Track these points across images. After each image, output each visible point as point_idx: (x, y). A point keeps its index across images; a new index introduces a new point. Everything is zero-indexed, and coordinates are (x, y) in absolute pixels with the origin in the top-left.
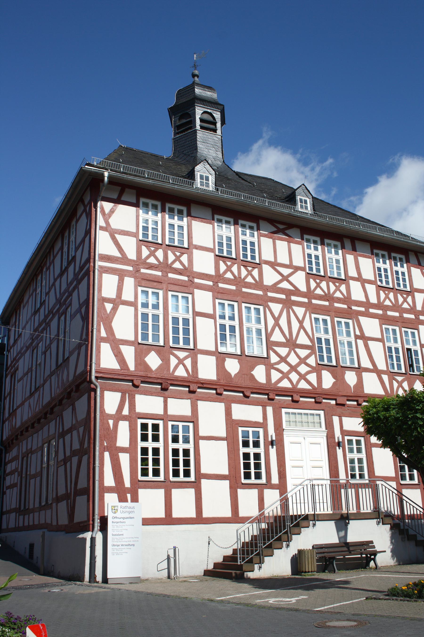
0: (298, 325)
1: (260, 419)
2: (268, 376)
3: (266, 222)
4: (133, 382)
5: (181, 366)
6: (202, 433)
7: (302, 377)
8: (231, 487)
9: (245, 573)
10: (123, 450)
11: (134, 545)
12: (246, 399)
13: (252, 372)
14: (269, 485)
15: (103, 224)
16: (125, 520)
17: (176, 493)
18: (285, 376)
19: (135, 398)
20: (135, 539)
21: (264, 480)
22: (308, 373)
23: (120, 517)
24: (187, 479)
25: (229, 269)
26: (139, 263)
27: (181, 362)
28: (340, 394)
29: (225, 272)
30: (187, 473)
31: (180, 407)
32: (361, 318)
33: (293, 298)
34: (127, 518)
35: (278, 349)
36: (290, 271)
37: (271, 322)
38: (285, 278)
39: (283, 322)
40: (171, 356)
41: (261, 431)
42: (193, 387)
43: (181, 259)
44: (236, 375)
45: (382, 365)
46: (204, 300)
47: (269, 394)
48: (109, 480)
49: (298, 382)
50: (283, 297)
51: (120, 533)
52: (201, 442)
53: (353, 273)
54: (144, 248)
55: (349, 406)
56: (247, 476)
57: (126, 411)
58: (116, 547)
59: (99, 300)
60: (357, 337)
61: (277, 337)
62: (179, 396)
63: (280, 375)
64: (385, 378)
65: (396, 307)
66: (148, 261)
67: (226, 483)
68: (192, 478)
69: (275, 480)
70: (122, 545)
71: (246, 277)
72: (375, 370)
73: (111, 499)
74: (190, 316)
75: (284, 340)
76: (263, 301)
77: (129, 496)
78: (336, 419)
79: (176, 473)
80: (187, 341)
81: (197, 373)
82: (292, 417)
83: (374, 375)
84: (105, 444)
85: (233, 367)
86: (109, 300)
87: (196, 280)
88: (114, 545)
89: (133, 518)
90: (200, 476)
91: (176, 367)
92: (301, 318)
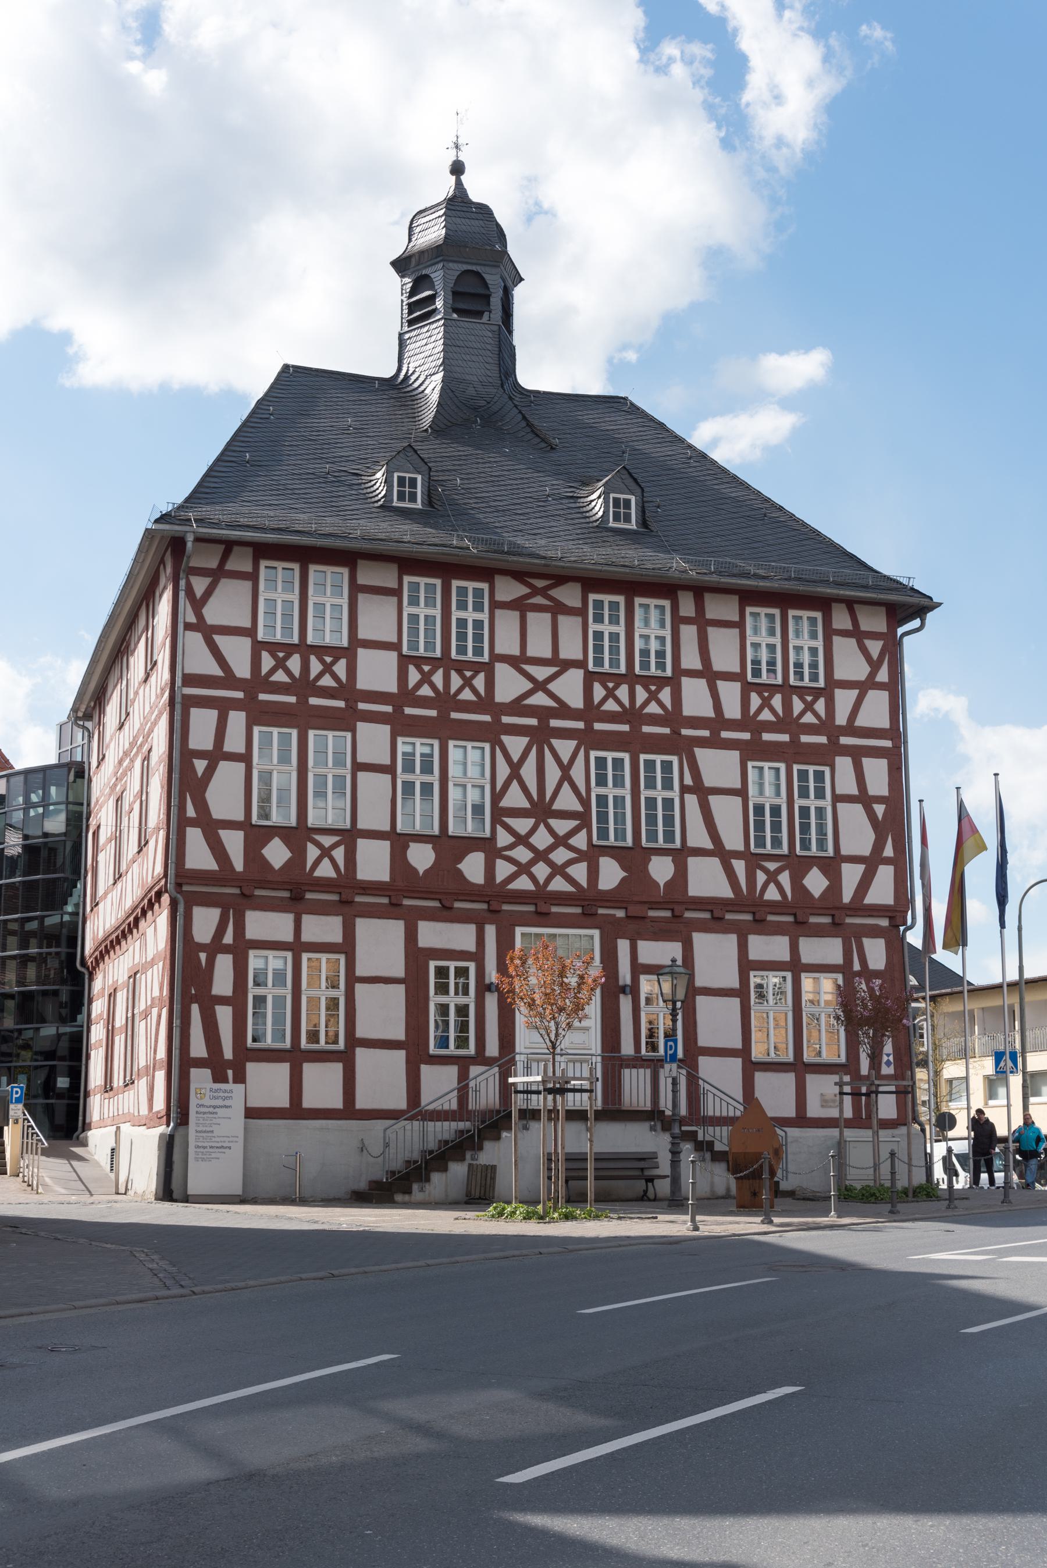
1: (471, 946)
2: (490, 870)
3: (509, 578)
7: (558, 870)
8: (408, 1061)
9: (892, 1072)
10: (223, 1000)
11: (230, 1148)
12: (446, 914)
13: (459, 866)
14: (481, 1058)
15: (192, 619)
16: (217, 1110)
18: (524, 869)
19: (244, 916)
20: (231, 1139)
21: (472, 1050)
22: (570, 862)
23: (208, 1104)
26: (258, 682)
27: (326, 853)
28: (636, 899)
29: (418, 685)
32: (699, 752)
33: (554, 723)
34: (221, 1107)
35: (514, 823)
38: (540, 686)
39: (528, 772)
40: (309, 844)
41: (472, 966)
43: (334, 668)
44: (426, 872)
45: (733, 841)
47: (494, 906)
49: (549, 879)
51: (208, 1129)
52: (359, 988)
53: (691, 660)
55: (654, 920)
56: (443, 1042)
57: (228, 939)
59: (182, 754)
60: (684, 789)
61: (514, 798)
63: (513, 869)
64: (739, 866)
65: (786, 722)
66: (273, 678)
69: (492, 1049)
70: (211, 1147)
71: (460, 690)
72: (719, 851)
74: (827, 803)
75: (527, 805)
77: (230, 1072)
78: (623, 946)
85: (421, 857)
86: (201, 754)
87: (362, 706)
88: (198, 1147)
91: (317, 862)
92: (565, 761)
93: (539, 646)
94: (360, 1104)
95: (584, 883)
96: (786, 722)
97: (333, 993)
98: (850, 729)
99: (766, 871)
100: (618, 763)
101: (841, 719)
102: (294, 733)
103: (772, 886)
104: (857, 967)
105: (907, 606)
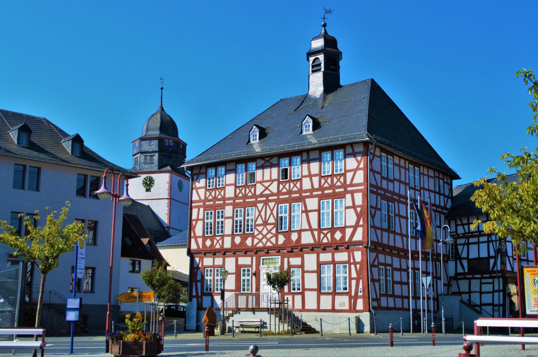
1: (250, 263)
2: (253, 242)
8: (318, 295)
10: (199, 281)
27: (218, 242)
31: (219, 261)
36: (270, 183)
41: (250, 268)
42: (224, 253)
50: (227, 202)
64: (316, 233)
65: (332, 186)
67: (316, 293)
76: (254, 204)
78: (286, 260)
90: (304, 289)
93: (267, 178)
94: (321, 308)
95: (275, 243)
96: (332, 186)
97: (345, 275)
98: (351, 185)
99: (323, 233)
100: (211, 213)
101: (348, 182)
102: (330, 200)
103: (325, 238)
104: (352, 261)
105: (37, 189)
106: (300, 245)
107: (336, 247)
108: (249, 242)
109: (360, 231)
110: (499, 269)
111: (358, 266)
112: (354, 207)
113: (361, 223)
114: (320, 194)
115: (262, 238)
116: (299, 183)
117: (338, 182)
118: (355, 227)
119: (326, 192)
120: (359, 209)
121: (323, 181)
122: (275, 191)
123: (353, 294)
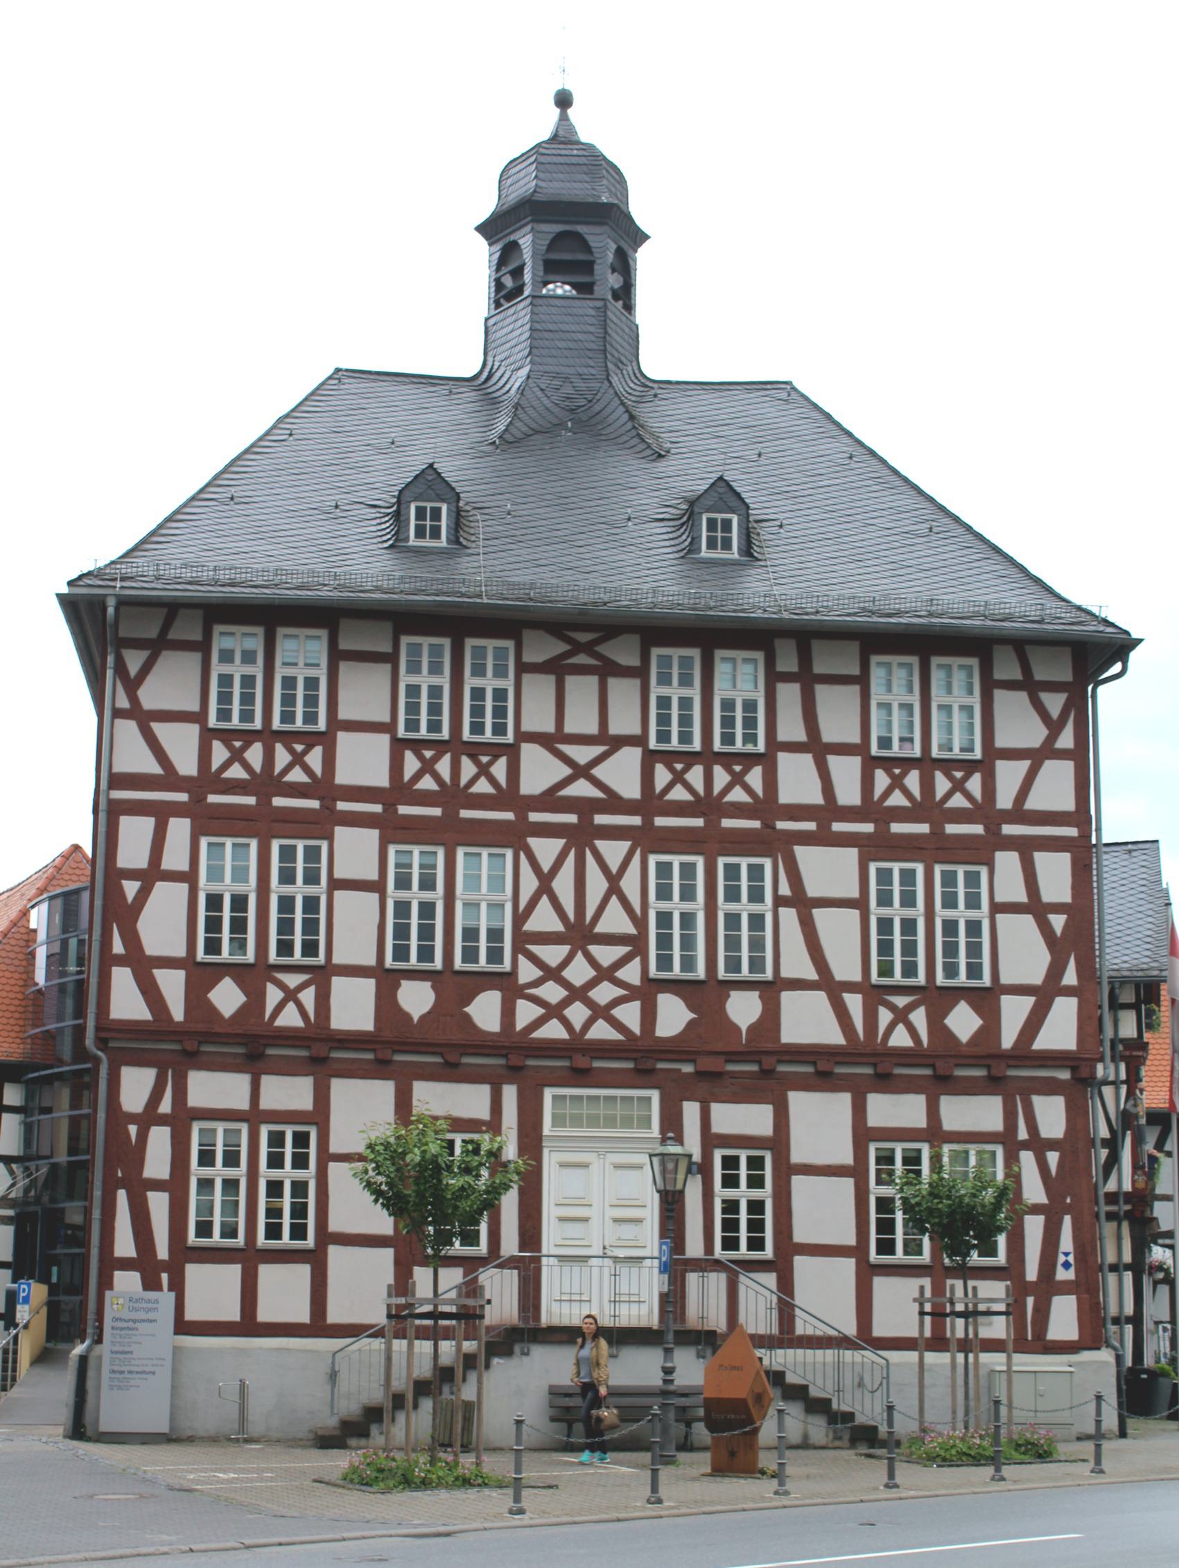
0: (604, 885)
2: (508, 1013)
3: (541, 633)
4: (182, 1045)
5: (291, 1006)
6: (334, 1148)
7: (601, 1012)
8: (397, 1262)
10: (157, 1185)
11: (154, 1373)
12: (450, 1072)
16: (137, 1325)
17: (267, 1274)
18: (554, 1011)
24: (298, 1244)
25: (428, 767)
27: (291, 995)
30: (299, 1232)
31: (288, 1092)
32: (799, 851)
36: (598, 750)
37: (529, 883)
42: (322, 1052)
44: (423, 1017)
45: (846, 967)
46: (355, 850)
48: (125, 1246)
51: (126, 1349)
54: (217, 746)
57: (165, 1107)
58: (118, 1375)
60: (779, 901)
61: (544, 919)
62: (288, 1069)
64: (854, 1003)
65: (926, 808)
68: (310, 1242)
73: (127, 1282)
76: (514, 837)
78: (691, 1111)
79: (274, 1231)
80: (757, 964)
81: (327, 1018)
82: (568, 1110)
83: (821, 997)
84: (120, 1174)
85: (416, 999)
86: (132, 874)
87: (342, 806)
88: (114, 1372)
89: (155, 1321)
93: (581, 719)
96: (926, 808)
98: (1019, 814)
99: (892, 1007)
101: (1005, 801)
104: (1023, 1134)
106: (769, 1046)
107: (939, 1069)
108: (485, 1011)
109: (1065, 1012)
110: (1127, 1186)
111: (1053, 1158)
112: (1036, 907)
113: (1070, 977)
114: (868, 835)
115: (566, 1003)
116: (318, 751)
117: (483, 780)
118: (1044, 995)
119: (897, 828)
120: (1058, 922)
121: (881, 780)
122: (630, 789)
123: (1032, 1274)
